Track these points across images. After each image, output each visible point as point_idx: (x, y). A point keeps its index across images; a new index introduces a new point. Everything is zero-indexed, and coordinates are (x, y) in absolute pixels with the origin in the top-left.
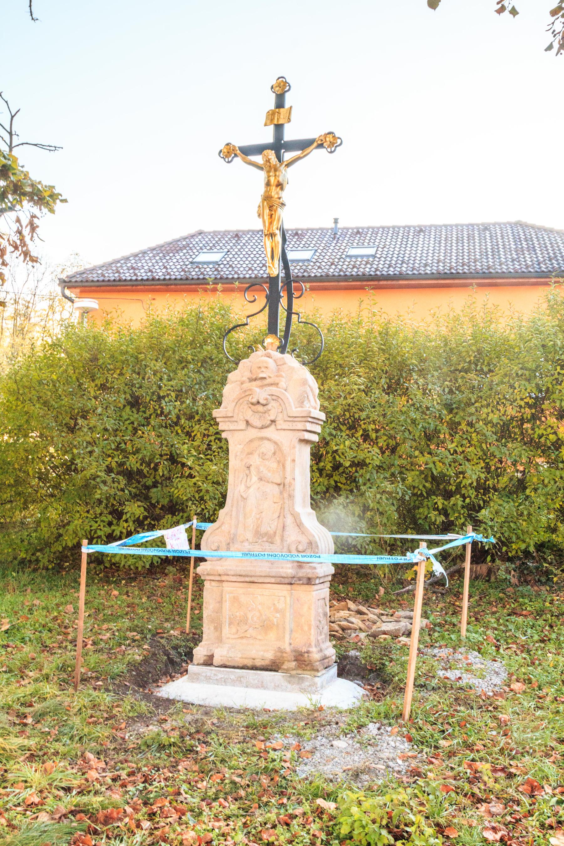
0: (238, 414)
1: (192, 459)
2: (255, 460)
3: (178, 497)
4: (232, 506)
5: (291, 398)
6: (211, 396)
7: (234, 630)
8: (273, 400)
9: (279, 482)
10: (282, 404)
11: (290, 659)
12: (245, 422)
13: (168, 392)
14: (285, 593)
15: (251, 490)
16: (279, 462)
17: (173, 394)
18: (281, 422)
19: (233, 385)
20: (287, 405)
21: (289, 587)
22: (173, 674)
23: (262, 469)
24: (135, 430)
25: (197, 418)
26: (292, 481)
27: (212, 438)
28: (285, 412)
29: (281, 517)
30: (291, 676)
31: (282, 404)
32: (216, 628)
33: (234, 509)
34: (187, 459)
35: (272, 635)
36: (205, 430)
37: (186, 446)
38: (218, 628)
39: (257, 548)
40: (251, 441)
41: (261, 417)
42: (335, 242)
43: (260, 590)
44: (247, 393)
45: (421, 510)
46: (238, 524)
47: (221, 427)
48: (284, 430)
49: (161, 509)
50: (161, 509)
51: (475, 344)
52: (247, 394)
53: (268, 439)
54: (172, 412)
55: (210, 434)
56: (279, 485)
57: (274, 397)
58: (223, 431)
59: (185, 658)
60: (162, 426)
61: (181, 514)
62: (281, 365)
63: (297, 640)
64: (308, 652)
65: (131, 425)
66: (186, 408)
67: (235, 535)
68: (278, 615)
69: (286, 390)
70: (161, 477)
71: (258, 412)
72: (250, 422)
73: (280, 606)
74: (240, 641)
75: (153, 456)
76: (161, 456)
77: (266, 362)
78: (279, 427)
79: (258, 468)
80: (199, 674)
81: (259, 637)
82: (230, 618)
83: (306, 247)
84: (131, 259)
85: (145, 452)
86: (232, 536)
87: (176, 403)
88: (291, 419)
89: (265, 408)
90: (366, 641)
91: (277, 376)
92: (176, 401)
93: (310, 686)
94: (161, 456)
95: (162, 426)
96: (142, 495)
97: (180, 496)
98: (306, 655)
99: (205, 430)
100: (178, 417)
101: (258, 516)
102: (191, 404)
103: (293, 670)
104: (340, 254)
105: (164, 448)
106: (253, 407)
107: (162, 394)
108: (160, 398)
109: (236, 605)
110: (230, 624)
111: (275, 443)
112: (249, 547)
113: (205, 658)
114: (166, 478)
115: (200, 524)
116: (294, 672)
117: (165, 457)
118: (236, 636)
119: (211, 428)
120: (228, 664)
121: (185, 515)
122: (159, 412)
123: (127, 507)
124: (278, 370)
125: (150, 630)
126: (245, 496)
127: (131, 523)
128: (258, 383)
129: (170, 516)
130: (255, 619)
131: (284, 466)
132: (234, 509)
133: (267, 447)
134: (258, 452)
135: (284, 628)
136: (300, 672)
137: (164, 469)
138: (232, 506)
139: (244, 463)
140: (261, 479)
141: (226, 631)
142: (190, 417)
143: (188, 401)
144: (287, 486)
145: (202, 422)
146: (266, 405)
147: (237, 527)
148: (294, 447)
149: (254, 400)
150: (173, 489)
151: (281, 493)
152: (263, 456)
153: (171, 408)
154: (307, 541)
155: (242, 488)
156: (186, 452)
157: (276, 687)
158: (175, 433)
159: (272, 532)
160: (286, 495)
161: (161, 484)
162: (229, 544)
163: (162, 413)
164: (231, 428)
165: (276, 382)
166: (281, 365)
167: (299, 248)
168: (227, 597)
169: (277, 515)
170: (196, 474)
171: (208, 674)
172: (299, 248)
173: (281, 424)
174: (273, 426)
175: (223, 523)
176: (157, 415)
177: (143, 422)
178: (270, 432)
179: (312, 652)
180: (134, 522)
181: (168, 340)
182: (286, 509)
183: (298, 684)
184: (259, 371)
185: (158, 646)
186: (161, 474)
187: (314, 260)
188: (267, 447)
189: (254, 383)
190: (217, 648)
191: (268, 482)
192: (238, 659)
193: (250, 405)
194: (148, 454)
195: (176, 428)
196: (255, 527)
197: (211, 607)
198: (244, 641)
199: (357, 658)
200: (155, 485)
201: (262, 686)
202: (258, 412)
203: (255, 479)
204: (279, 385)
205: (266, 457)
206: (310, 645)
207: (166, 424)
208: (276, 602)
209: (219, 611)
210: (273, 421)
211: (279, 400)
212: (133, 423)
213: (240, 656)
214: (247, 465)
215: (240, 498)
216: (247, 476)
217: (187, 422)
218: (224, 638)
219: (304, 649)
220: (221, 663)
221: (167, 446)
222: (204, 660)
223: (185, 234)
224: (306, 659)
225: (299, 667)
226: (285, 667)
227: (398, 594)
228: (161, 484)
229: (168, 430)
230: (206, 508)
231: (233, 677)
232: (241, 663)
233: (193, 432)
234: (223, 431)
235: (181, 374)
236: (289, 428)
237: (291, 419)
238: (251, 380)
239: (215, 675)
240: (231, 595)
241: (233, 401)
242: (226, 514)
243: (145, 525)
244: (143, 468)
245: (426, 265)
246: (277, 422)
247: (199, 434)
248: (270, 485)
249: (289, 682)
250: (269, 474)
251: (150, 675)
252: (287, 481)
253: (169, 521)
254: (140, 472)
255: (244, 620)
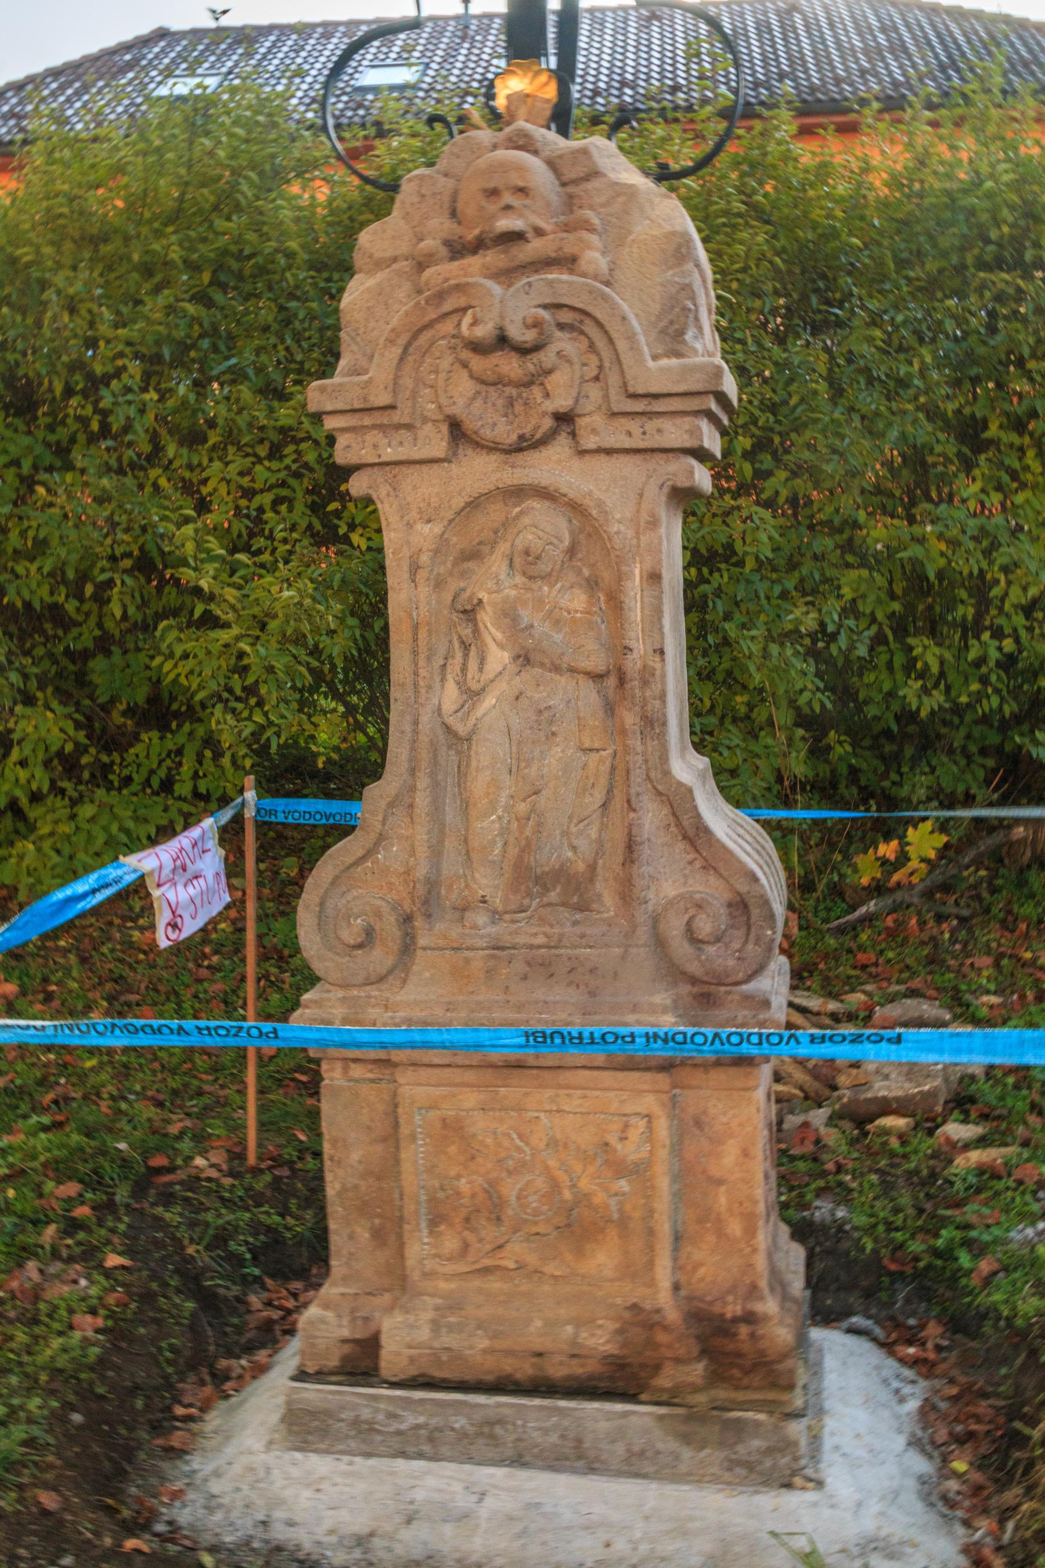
0: (414, 394)
1: (211, 568)
2: (495, 583)
3: (175, 681)
4: (413, 771)
5: (632, 312)
6: (251, 372)
7: (450, 1243)
8: (561, 326)
9: (601, 668)
10: (601, 344)
11: (682, 1352)
12: (445, 428)
13: (120, 363)
14: (649, 1102)
15: (489, 701)
16: (592, 585)
17: (135, 368)
18: (598, 420)
19: (380, 276)
20: (621, 345)
21: (662, 1080)
22: (223, 1363)
23: (526, 615)
24: (29, 483)
25: (213, 438)
26: (655, 662)
27: (266, 499)
28: (613, 379)
29: (618, 802)
30: (693, 1417)
31: (601, 344)
32: (378, 1236)
33: (423, 782)
34: (195, 569)
35: (603, 1259)
36: (241, 474)
37: (189, 530)
38: (389, 1233)
39: (528, 933)
40: (474, 504)
41: (511, 402)
42: (466, 45)
43: (549, 1093)
44: (444, 303)
45: (870, 677)
46: (441, 842)
47: (342, 456)
48: (609, 452)
49: (124, 714)
50: (124, 714)
51: (1017, 186)
52: (447, 307)
53: (544, 493)
54: (138, 426)
55: (258, 486)
56: (598, 677)
57: (566, 317)
58: (358, 467)
59: (257, 1272)
60: (109, 469)
61: (187, 727)
62: (575, 182)
63: (702, 1271)
64: (750, 1318)
65: (13, 470)
66: (175, 411)
67: (432, 884)
68: (624, 1185)
69: (607, 284)
70: (118, 624)
71: (499, 382)
72: (470, 425)
73: (632, 1150)
74: (477, 1283)
75: (89, 556)
76: (113, 558)
77: (521, 168)
78: (590, 442)
79: (509, 615)
80: (327, 1413)
81: (551, 1268)
82: (432, 1200)
83: (403, 60)
84: (10, 94)
85: (63, 552)
86: (421, 890)
87: (147, 397)
88: (640, 406)
89: (530, 365)
90: (832, 1137)
91: (567, 228)
92: (145, 390)
93: (769, 1451)
94: (113, 558)
95: (109, 469)
96: (70, 682)
97: (183, 680)
98: (744, 1330)
99: (241, 474)
100: (154, 438)
101: (522, 808)
102: (192, 397)
103: (696, 1389)
104: (480, 70)
105: (120, 536)
106: (477, 363)
107: (98, 369)
108: (96, 383)
109: (453, 1149)
110: (434, 1222)
111: (575, 508)
112: (492, 930)
113: (347, 1349)
114: (135, 625)
115: (268, 802)
116: (701, 1399)
117: (127, 563)
118: (462, 1267)
119: (258, 468)
120: (437, 1374)
121: (201, 731)
122: (95, 426)
123: (23, 724)
124: (570, 203)
125: (125, 1163)
126: (462, 730)
127: (39, 772)
128: (492, 258)
129: (155, 734)
130: (533, 1201)
131: (616, 604)
132: (423, 782)
133: (543, 527)
134: (504, 547)
135: (651, 1232)
136: (722, 1394)
137: (127, 600)
138: (413, 771)
139: (448, 597)
140: (524, 659)
141: (419, 1248)
142: (193, 439)
143: (182, 390)
144: (634, 684)
145: (231, 449)
146: (537, 348)
147: (436, 853)
148: (654, 523)
149: (484, 331)
150: (158, 660)
151: (610, 709)
152: (529, 564)
153: (132, 412)
154: (727, 896)
155: (450, 696)
156: (190, 547)
157: (635, 1465)
158: (148, 489)
159: (581, 867)
160: (630, 719)
161: (121, 644)
162: (408, 919)
163: (105, 430)
164: (389, 453)
165: (568, 250)
166: (575, 182)
167: (388, 62)
168: (415, 1122)
169: (599, 797)
170: (231, 616)
171: (366, 1414)
172: (388, 62)
173: (598, 428)
174: (563, 439)
175: (381, 838)
176: (92, 439)
177: (48, 459)
178: (553, 466)
179: (766, 1318)
180: (47, 764)
181: (109, 204)
182: (637, 776)
183: (722, 1444)
184: (492, 207)
185: (158, 1244)
186: (118, 614)
187: (425, 86)
188: (543, 527)
189: (474, 262)
190: (390, 1309)
191: (557, 669)
192: (475, 1349)
193: (465, 354)
194: (74, 557)
195: (154, 473)
196: (513, 852)
197: (355, 1156)
198: (495, 1284)
199: (840, 1229)
200: (104, 644)
201: (577, 1458)
202: (499, 382)
203: (498, 658)
204: (583, 265)
205: (544, 567)
206: (753, 1291)
207: (119, 459)
208: (612, 1139)
209: (389, 1169)
210: (565, 419)
211: (589, 328)
212: (16, 463)
213: (485, 1343)
214: (463, 603)
215: (440, 731)
216: (466, 647)
217: (184, 451)
218: (415, 1276)
219: (733, 1309)
220: (413, 1371)
221: (127, 530)
222: (345, 1359)
223: (127, 35)
224: (746, 1347)
225: (716, 1377)
226: (664, 1380)
227: (841, 931)
228: (121, 644)
229: (129, 481)
230: (271, 723)
231: (460, 1422)
232: (490, 1367)
233: (205, 482)
234: (358, 467)
235: (154, 306)
236: (628, 443)
237: (640, 406)
238: (458, 250)
239: (392, 1416)
240: (433, 1114)
241: (391, 342)
242: (391, 805)
243: (82, 768)
244: (61, 599)
245: (675, 89)
246: (582, 422)
247: (223, 489)
248: (563, 681)
249: (687, 1439)
250: (558, 637)
251: (139, 1404)
252: (633, 664)
253: (154, 751)
254: (55, 612)
255: (492, 1205)
